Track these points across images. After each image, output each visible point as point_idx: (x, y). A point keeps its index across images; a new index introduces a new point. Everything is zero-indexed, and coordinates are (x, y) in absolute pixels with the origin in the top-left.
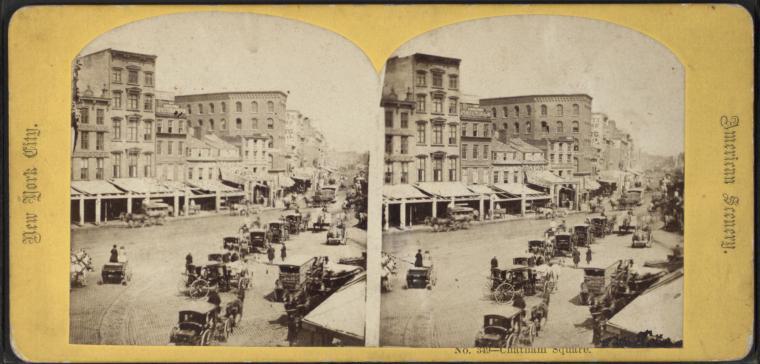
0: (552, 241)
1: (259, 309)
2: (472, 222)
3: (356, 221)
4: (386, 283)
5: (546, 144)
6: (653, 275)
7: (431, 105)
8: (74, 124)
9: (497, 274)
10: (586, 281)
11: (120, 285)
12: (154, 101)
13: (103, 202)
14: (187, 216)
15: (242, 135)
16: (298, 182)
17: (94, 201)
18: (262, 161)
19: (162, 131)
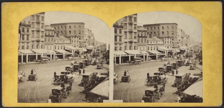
0: (73, 67)
1: (170, 90)
2: (141, 62)
3: (199, 62)
4: (115, 81)
5: (163, 38)
6: (197, 78)
7: (128, 27)
8: (20, 32)
9: (149, 77)
10: (176, 80)
11: (34, 81)
12: (44, 26)
13: (122, 57)
14: (54, 60)
15: (164, 37)
16: (181, 51)
17: (26, 56)
18: (77, 44)
19: (139, 36)
